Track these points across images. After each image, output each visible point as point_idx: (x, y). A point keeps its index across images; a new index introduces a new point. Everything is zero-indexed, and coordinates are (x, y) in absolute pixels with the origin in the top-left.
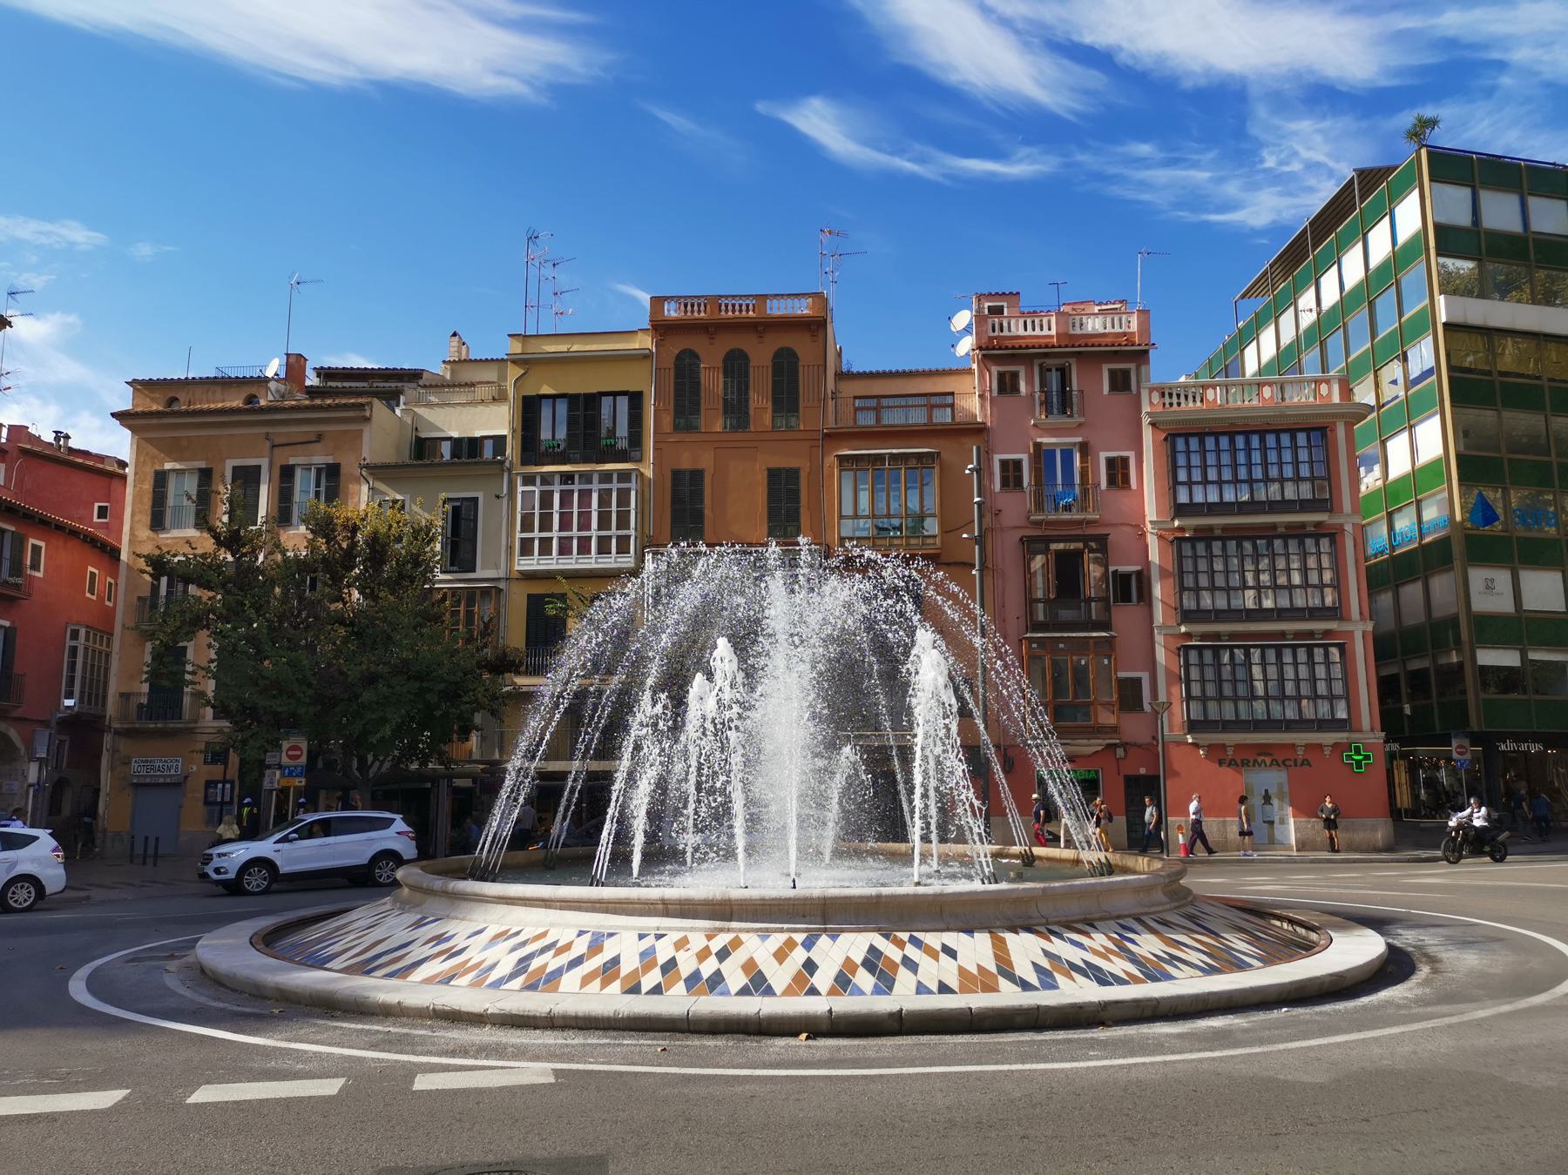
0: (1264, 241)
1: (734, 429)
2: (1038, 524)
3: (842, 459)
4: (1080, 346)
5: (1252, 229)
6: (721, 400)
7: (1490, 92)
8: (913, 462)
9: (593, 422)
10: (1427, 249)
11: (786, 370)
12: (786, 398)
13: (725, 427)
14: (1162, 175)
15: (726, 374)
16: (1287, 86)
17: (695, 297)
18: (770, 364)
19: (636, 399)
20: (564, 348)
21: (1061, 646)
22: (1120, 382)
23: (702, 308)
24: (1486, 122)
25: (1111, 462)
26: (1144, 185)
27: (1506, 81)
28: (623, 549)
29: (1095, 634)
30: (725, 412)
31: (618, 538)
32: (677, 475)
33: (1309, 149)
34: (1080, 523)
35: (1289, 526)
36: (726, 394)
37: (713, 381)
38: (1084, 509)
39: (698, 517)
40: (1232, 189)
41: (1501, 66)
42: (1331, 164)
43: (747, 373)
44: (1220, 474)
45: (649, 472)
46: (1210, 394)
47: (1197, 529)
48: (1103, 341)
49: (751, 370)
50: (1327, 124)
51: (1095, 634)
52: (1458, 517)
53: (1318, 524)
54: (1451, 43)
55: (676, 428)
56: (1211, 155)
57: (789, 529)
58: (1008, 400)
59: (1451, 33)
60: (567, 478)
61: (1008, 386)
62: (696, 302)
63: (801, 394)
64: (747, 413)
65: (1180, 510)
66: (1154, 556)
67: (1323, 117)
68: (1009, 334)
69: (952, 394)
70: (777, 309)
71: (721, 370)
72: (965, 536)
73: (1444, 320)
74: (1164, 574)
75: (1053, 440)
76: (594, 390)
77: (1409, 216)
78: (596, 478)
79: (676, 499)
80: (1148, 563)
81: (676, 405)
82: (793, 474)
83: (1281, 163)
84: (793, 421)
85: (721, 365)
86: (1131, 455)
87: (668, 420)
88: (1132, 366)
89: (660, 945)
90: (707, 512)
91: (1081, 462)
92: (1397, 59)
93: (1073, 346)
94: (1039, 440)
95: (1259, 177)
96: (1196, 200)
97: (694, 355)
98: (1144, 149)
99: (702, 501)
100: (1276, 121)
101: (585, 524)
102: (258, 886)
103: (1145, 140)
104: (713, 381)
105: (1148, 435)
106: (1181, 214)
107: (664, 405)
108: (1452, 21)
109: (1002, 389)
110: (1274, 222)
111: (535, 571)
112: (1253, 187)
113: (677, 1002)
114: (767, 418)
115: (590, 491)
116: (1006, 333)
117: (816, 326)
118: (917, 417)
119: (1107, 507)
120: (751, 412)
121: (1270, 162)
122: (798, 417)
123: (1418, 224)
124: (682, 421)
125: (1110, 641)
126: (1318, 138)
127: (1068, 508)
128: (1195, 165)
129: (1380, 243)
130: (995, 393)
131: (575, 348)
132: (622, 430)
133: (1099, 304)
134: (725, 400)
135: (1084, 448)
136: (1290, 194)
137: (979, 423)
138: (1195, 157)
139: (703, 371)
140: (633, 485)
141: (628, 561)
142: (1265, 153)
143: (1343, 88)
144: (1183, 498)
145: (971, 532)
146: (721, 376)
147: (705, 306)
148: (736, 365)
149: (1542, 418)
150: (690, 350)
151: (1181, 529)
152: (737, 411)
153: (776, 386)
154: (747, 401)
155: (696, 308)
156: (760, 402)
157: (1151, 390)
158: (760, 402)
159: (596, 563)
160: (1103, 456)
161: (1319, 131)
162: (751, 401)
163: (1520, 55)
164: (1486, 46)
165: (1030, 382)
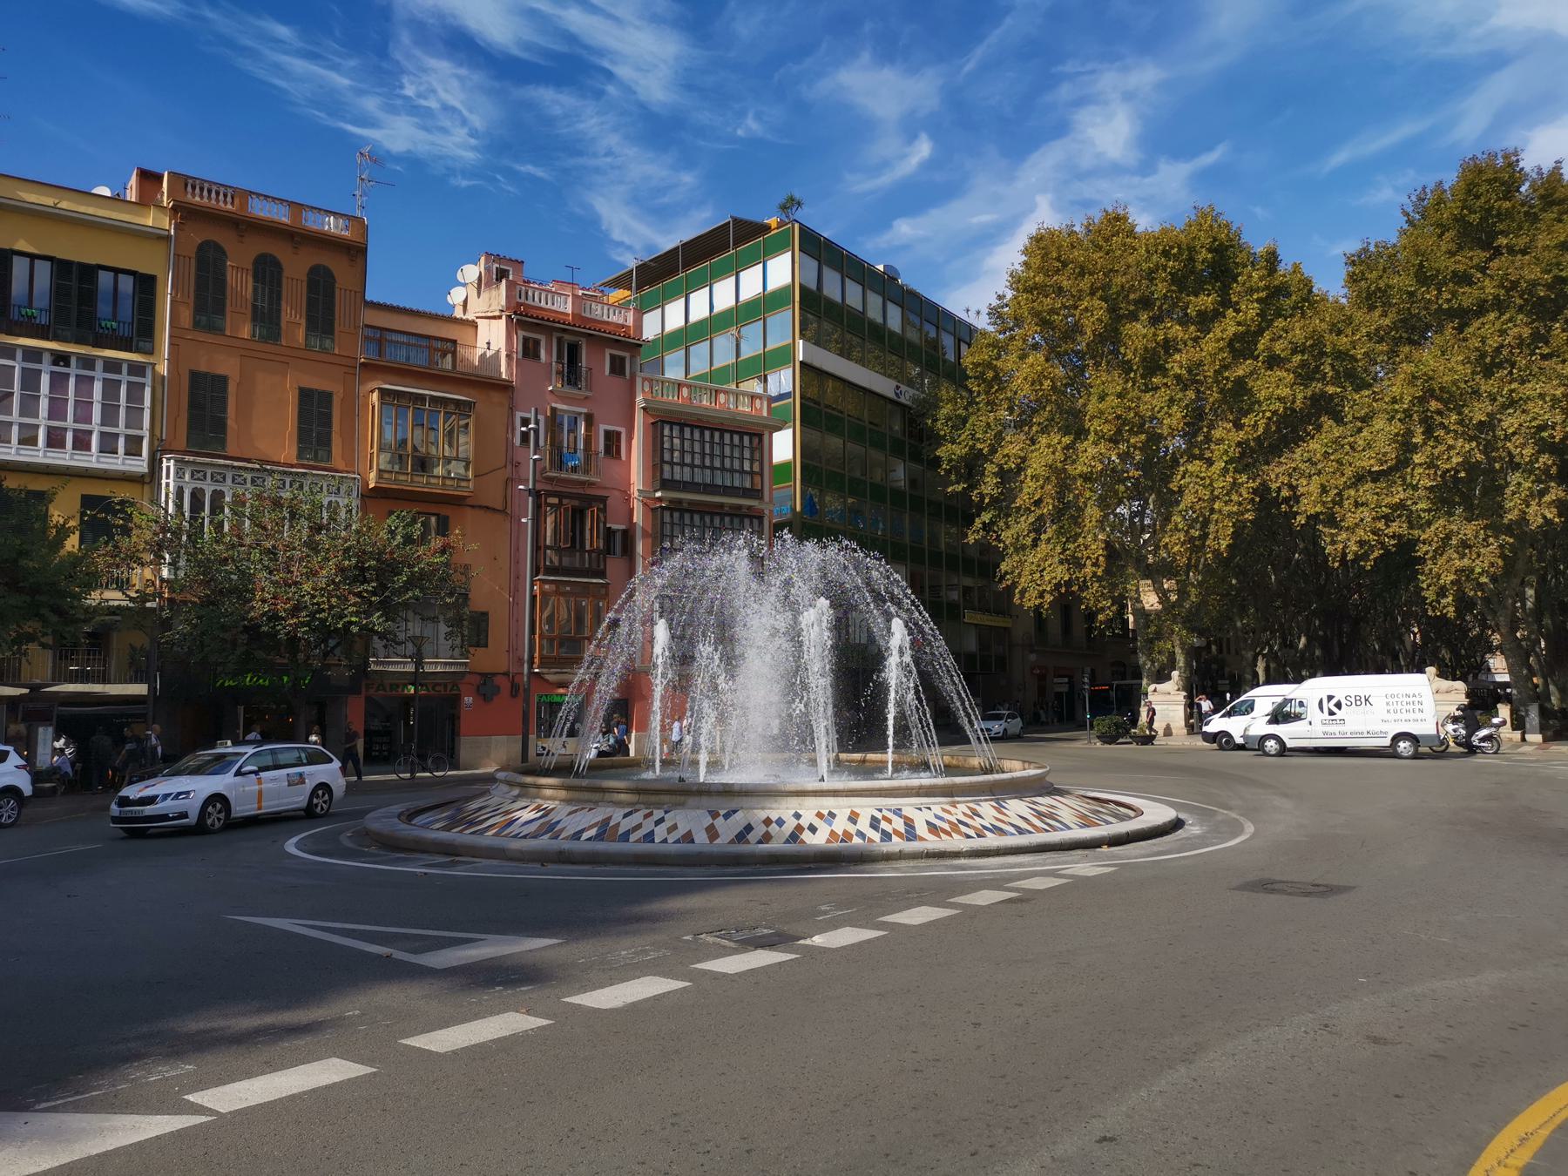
0: (398, 168)
1: (264, 339)
2: (550, 480)
3: (383, 392)
4: (589, 329)
5: (388, 152)
6: (249, 306)
7: (599, 94)
8: (451, 408)
9: (88, 296)
10: (794, 302)
11: (321, 290)
12: (321, 319)
13: (254, 336)
14: (299, 65)
15: (256, 278)
16: (431, 21)
17: (223, 185)
18: (305, 278)
19: (146, 284)
20: (50, 201)
21: (568, 588)
22: (618, 367)
23: (229, 199)
24: (594, 121)
25: (608, 434)
26: (278, 68)
27: (611, 89)
28: (133, 448)
29: (594, 581)
30: (254, 319)
31: (128, 437)
32: (196, 377)
33: (446, 91)
34: (583, 483)
35: (733, 507)
36: (255, 300)
37: (240, 284)
38: (587, 472)
39: (220, 426)
40: (371, 104)
41: (610, 76)
42: (465, 112)
43: (279, 284)
44: (693, 459)
45: (163, 369)
46: (722, 398)
47: (671, 501)
48: (603, 327)
49: (284, 281)
50: (463, 71)
51: (594, 581)
52: (798, 508)
53: (749, 508)
54: (571, 38)
55: (196, 324)
56: (352, 63)
57: (320, 453)
58: (529, 363)
59: (573, 29)
60: (61, 359)
61: (531, 352)
62: (230, 191)
63: (337, 316)
64: (278, 324)
65: (665, 484)
66: (638, 517)
67: (461, 65)
68: (532, 303)
69: (454, 342)
70: (260, 210)
71: (250, 273)
72: (521, 487)
73: (801, 359)
74: (645, 534)
75: (565, 407)
76: (93, 262)
77: (780, 271)
78: (99, 365)
79: (195, 405)
80: (632, 525)
81: (197, 297)
82: (326, 397)
83: (420, 96)
84: (327, 343)
85: (250, 267)
86: (623, 430)
87: (186, 316)
88: (627, 355)
89: (657, 830)
90: (230, 423)
91: (586, 430)
92: (529, 35)
93: (584, 328)
94: (554, 405)
95: (399, 102)
96: (332, 103)
97: (277, 265)
98: (283, 31)
99: (224, 410)
100: (418, 52)
101: (83, 414)
102: (9, 817)
103: (286, 23)
104: (240, 284)
105: (639, 418)
106: (317, 113)
107: (182, 295)
108: (575, 19)
109: (526, 353)
110: (409, 151)
111: (68, 467)
112: (392, 110)
113: (992, 841)
114: (301, 334)
115: (92, 379)
116: (530, 302)
117: (355, 251)
118: (419, 359)
119: (602, 475)
120: (283, 325)
121: (409, 91)
122: (333, 340)
123: (789, 280)
124: (204, 318)
125: (606, 586)
126: (455, 83)
127: (574, 469)
128: (335, 67)
129: (751, 283)
130: (520, 356)
131: (64, 205)
132: (127, 310)
133: (582, 289)
134: (255, 307)
135: (589, 419)
136: (426, 129)
137: (504, 380)
138: (338, 60)
139: (229, 269)
140: (148, 380)
141: (140, 465)
142: (405, 80)
143: (482, 44)
144: (667, 476)
145: (525, 482)
146: (250, 279)
147: (233, 198)
148: (267, 272)
149: (842, 441)
150: (214, 242)
151: (660, 499)
152: (267, 319)
153: (311, 304)
154: (279, 311)
155: (221, 197)
156: (293, 318)
157: (644, 379)
158: (293, 318)
159: (98, 462)
160: (603, 428)
161: (459, 77)
162: (283, 314)
163: (623, 71)
164: (601, 52)
165: (549, 352)
